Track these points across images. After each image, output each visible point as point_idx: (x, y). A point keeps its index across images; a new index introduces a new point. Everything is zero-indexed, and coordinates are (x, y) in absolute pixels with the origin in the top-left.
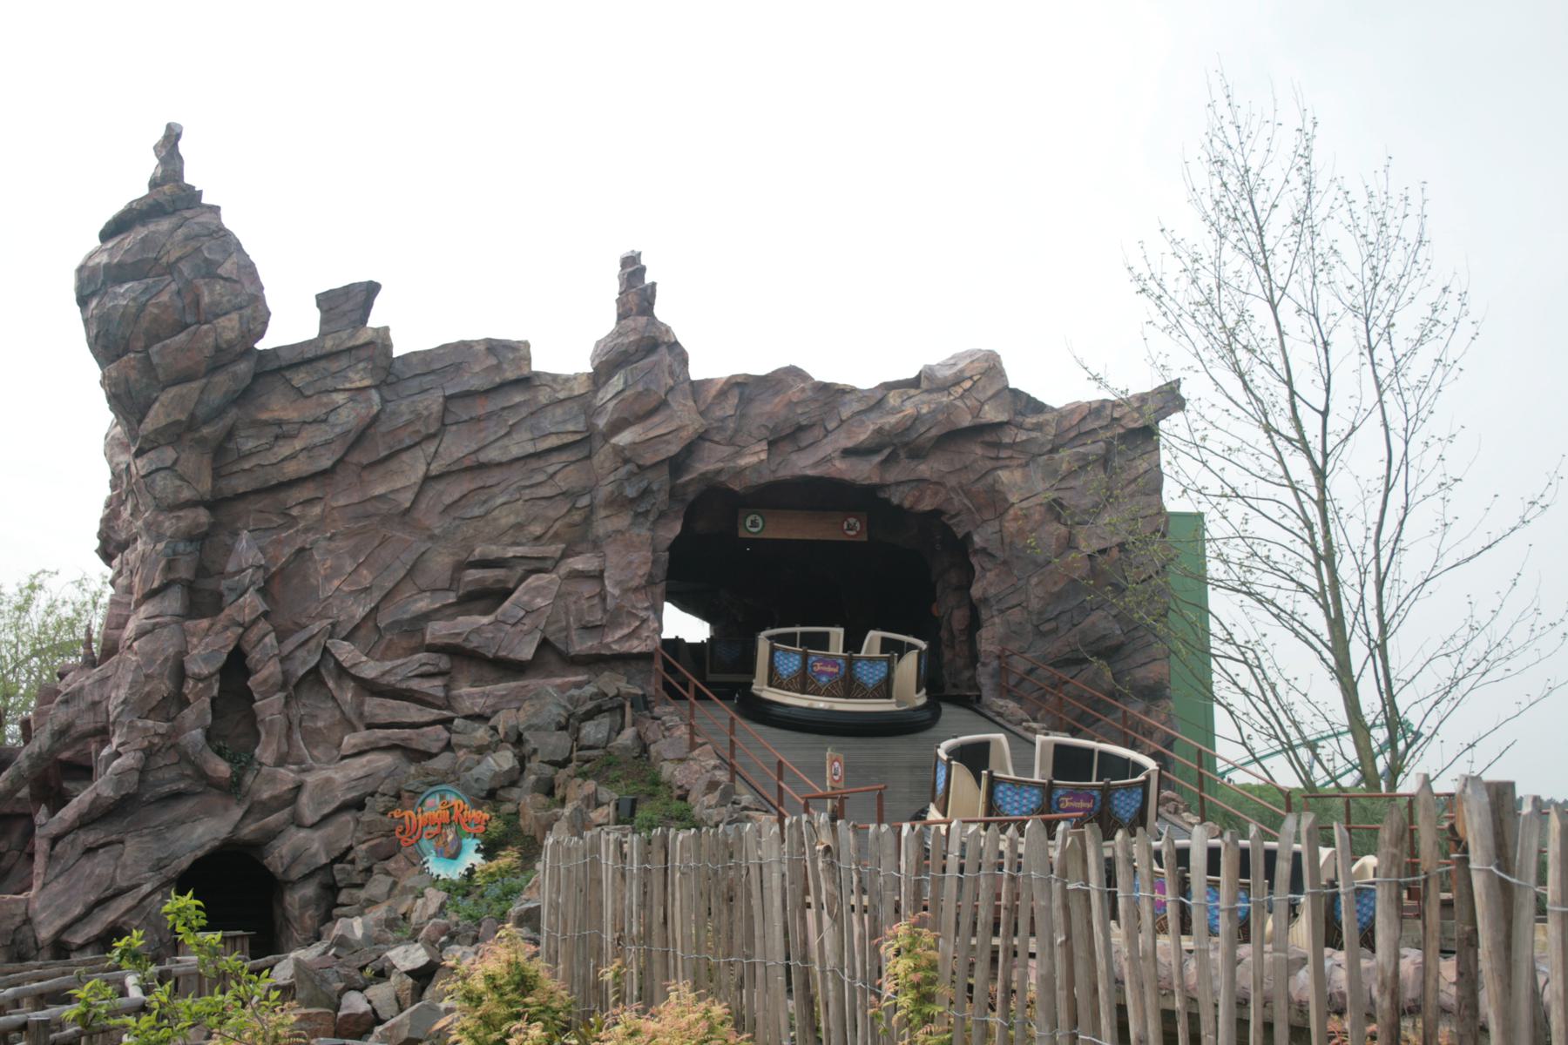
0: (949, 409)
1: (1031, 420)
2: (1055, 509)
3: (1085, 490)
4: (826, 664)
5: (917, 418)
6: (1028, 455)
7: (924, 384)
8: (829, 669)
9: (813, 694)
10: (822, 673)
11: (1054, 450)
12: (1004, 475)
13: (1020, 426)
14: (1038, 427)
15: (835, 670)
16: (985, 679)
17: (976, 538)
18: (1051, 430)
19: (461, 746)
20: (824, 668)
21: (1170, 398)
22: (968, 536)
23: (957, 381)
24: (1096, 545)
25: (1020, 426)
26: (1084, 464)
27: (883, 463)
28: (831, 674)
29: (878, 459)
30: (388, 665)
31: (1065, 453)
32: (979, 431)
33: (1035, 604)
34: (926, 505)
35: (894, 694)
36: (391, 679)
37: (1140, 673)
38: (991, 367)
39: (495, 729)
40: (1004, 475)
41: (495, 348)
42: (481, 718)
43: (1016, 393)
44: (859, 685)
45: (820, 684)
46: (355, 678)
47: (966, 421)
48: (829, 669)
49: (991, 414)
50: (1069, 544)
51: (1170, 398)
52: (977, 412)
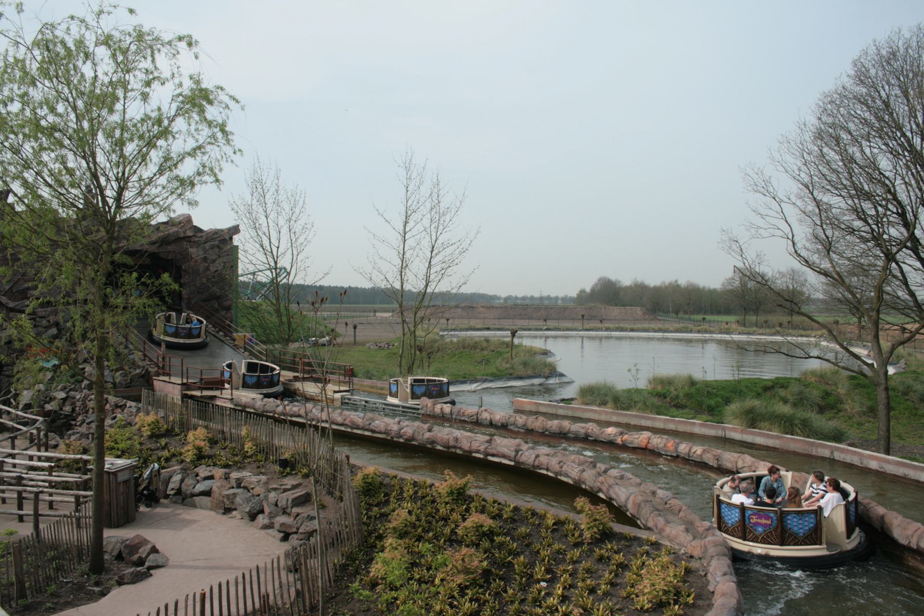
0: (177, 232)
1: (199, 235)
2: (205, 259)
3: (212, 255)
4: (760, 517)
5: (169, 235)
6: (198, 244)
7: (170, 224)
8: (763, 521)
9: (752, 541)
10: (756, 524)
11: (205, 243)
12: (191, 250)
13: (196, 236)
14: (201, 237)
15: (769, 522)
16: (183, 305)
17: (183, 267)
18: (204, 238)
19: (39, 326)
20: (759, 521)
21: (235, 230)
22: (181, 266)
23: (180, 223)
24: (215, 269)
25: (196, 236)
26: (212, 247)
27: (158, 247)
28: (765, 525)
29: (157, 245)
30: (17, 303)
31: (208, 244)
32: (187, 239)
33: (198, 285)
34: (170, 258)
35: (824, 540)
36: (18, 307)
37: (224, 303)
38: (676, 281)
39: (49, 321)
40: (191, 250)
41: (600, 280)
42: (43, 317)
43: (195, 227)
44: (791, 535)
45: (757, 533)
46: (7, 307)
47: (182, 235)
48: (763, 521)
49: (189, 233)
50: (208, 269)
51: (235, 230)
52: (185, 233)
